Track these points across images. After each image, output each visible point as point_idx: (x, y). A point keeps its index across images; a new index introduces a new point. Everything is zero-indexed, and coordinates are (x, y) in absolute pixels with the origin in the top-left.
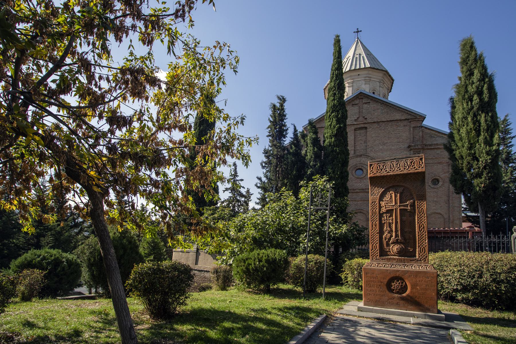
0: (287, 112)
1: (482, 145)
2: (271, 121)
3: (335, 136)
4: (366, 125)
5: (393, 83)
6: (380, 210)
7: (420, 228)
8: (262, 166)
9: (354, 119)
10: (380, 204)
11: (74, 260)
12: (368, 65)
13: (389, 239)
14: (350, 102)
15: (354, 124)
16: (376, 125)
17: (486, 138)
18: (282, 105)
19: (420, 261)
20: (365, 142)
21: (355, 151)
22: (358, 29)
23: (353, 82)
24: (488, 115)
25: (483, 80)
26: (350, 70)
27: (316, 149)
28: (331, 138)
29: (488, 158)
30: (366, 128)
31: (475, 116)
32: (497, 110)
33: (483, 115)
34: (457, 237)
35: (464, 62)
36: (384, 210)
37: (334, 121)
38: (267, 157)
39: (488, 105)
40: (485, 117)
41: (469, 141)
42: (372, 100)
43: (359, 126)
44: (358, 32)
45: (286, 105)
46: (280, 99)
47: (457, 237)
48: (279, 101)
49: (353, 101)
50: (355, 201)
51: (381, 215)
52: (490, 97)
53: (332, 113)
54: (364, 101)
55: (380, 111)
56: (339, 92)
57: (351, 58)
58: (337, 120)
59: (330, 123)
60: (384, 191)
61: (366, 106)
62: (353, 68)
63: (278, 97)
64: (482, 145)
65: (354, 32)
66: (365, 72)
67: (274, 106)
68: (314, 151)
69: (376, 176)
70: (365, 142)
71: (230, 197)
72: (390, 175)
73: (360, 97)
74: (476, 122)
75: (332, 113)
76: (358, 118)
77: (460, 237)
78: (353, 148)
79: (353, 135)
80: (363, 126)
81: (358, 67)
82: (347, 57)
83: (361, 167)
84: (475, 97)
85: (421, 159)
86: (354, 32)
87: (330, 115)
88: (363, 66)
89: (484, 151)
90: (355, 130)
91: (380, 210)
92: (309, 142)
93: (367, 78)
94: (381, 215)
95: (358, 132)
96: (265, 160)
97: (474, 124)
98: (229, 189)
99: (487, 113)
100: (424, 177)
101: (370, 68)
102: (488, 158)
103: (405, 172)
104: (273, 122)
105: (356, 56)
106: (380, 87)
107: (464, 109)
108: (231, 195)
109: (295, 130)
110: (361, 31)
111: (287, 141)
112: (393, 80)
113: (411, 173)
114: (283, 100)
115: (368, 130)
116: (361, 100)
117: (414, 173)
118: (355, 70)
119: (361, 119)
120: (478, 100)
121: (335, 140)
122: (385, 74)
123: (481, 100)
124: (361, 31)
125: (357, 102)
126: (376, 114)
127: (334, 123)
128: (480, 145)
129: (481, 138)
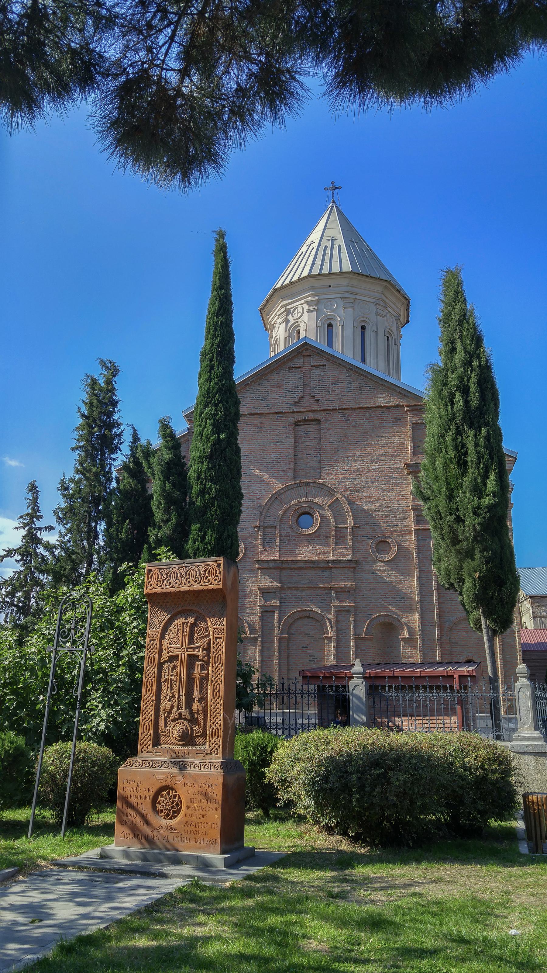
0: (119, 395)
1: (467, 494)
2: (84, 415)
3: (210, 457)
4: (318, 416)
5: (408, 305)
6: (160, 656)
7: (214, 690)
8: (59, 518)
9: (292, 400)
10: (161, 645)
11: (446, 89)
12: (347, 267)
13: (170, 712)
14: (284, 363)
15: (293, 412)
16: (337, 416)
17: (476, 479)
18: (108, 382)
19: (211, 753)
20: (318, 452)
21: (295, 471)
22: (333, 183)
23: (317, 303)
24: (480, 433)
25: (470, 363)
26: (309, 276)
27: (168, 486)
28: (202, 463)
29: (476, 521)
30: (318, 421)
31: (459, 433)
32: (500, 423)
33: (471, 433)
34: (424, 687)
35: (446, 321)
36: (165, 656)
37: (207, 426)
38: (69, 497)
39: (481, 413)
40: (476, 436)
41: (448, 484)
42: (328, 360)
43: (303, 417)
44: (334, 188)
45: (119, 383)
46: (108, 369)
47: (424, 687)
48: (104, 372)
49: (291, 360)
50: (297, 588)
51: (160, 665)
52: (482, 397)
53: (206, 406)
54: (314, 361)
55: (345, 385)
56: (220, 363)
57: (315, 245)
58: (214, 425)
59: (200, 429)
60: (169, 619)
61: (316, 372)
62: (316, 271)
63: (102, 363)
64: (467, 494)
65: (326, 189)
66: (344, 281)
67: (94, 381)
68: (164, 491)
69: (155, 593)
70: (318, 452)
71: (19, 573)
72: (175, 593)
73: (305, 353)
74: (460, 448)
75: (206, 406)
76: (301, 398)
77: (431, 687)
78: (292, 465)
79: (292, 436)
80: (311, 416)
81: (326, 270)
82: (308, 242)
83: (307, 510)
84: (458, 396)
85: (219, 565)
86: (326, 189)
87: (201, 413)
88: (336, 269)
89: (470, 507)
90: (297, 424)
91: (160, 656)
92: (156, 468)
93: (347, 295)
94: (160, 665)
95: (302, 428)
96: (63, 505)
97: (456, 448)
98: (16, 551)
99: (478, 430)
100: (224, 597)
101: (352, 272)
102: (476, 521)
103: (196, 587)
104: (87, 417)
105: (325, 243)
106: (377, 314)
107: (440, 417)
108: (19, 567)
109: (136, 439)
110: (340, 188)
111: (119, 459)
112: (408, 300)
113: (203, 591)
114: (113, 371)
115: (322, 425)
116: (307, 359)
117: (209, 591)
118: (319, 275)
119: (307, 400)
120: (462, 403)
121: (209, 468)
122: (386, 288)
123: (467, 402)
124: (340, 188)
125: (298, 362)
126: (338, 391)
127: (208, 430)
128: (464, 493)
129: (467, 480)
